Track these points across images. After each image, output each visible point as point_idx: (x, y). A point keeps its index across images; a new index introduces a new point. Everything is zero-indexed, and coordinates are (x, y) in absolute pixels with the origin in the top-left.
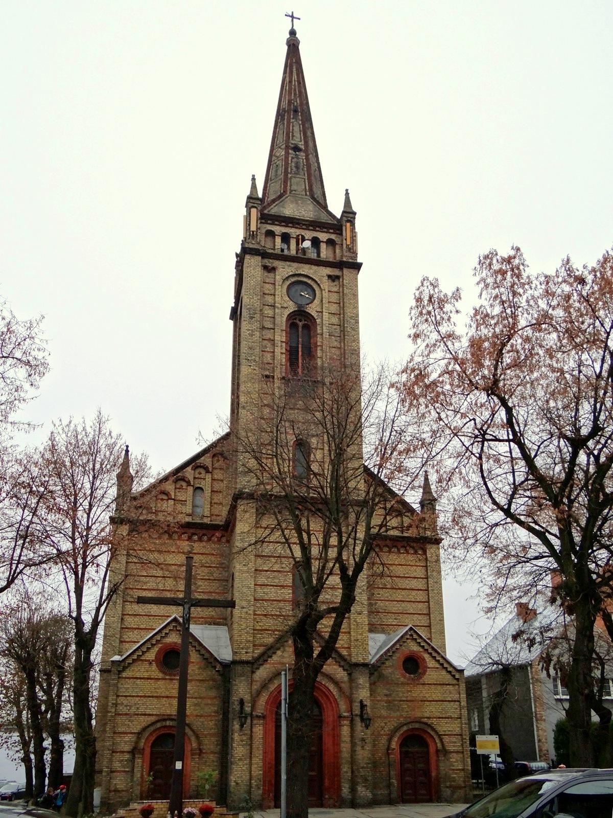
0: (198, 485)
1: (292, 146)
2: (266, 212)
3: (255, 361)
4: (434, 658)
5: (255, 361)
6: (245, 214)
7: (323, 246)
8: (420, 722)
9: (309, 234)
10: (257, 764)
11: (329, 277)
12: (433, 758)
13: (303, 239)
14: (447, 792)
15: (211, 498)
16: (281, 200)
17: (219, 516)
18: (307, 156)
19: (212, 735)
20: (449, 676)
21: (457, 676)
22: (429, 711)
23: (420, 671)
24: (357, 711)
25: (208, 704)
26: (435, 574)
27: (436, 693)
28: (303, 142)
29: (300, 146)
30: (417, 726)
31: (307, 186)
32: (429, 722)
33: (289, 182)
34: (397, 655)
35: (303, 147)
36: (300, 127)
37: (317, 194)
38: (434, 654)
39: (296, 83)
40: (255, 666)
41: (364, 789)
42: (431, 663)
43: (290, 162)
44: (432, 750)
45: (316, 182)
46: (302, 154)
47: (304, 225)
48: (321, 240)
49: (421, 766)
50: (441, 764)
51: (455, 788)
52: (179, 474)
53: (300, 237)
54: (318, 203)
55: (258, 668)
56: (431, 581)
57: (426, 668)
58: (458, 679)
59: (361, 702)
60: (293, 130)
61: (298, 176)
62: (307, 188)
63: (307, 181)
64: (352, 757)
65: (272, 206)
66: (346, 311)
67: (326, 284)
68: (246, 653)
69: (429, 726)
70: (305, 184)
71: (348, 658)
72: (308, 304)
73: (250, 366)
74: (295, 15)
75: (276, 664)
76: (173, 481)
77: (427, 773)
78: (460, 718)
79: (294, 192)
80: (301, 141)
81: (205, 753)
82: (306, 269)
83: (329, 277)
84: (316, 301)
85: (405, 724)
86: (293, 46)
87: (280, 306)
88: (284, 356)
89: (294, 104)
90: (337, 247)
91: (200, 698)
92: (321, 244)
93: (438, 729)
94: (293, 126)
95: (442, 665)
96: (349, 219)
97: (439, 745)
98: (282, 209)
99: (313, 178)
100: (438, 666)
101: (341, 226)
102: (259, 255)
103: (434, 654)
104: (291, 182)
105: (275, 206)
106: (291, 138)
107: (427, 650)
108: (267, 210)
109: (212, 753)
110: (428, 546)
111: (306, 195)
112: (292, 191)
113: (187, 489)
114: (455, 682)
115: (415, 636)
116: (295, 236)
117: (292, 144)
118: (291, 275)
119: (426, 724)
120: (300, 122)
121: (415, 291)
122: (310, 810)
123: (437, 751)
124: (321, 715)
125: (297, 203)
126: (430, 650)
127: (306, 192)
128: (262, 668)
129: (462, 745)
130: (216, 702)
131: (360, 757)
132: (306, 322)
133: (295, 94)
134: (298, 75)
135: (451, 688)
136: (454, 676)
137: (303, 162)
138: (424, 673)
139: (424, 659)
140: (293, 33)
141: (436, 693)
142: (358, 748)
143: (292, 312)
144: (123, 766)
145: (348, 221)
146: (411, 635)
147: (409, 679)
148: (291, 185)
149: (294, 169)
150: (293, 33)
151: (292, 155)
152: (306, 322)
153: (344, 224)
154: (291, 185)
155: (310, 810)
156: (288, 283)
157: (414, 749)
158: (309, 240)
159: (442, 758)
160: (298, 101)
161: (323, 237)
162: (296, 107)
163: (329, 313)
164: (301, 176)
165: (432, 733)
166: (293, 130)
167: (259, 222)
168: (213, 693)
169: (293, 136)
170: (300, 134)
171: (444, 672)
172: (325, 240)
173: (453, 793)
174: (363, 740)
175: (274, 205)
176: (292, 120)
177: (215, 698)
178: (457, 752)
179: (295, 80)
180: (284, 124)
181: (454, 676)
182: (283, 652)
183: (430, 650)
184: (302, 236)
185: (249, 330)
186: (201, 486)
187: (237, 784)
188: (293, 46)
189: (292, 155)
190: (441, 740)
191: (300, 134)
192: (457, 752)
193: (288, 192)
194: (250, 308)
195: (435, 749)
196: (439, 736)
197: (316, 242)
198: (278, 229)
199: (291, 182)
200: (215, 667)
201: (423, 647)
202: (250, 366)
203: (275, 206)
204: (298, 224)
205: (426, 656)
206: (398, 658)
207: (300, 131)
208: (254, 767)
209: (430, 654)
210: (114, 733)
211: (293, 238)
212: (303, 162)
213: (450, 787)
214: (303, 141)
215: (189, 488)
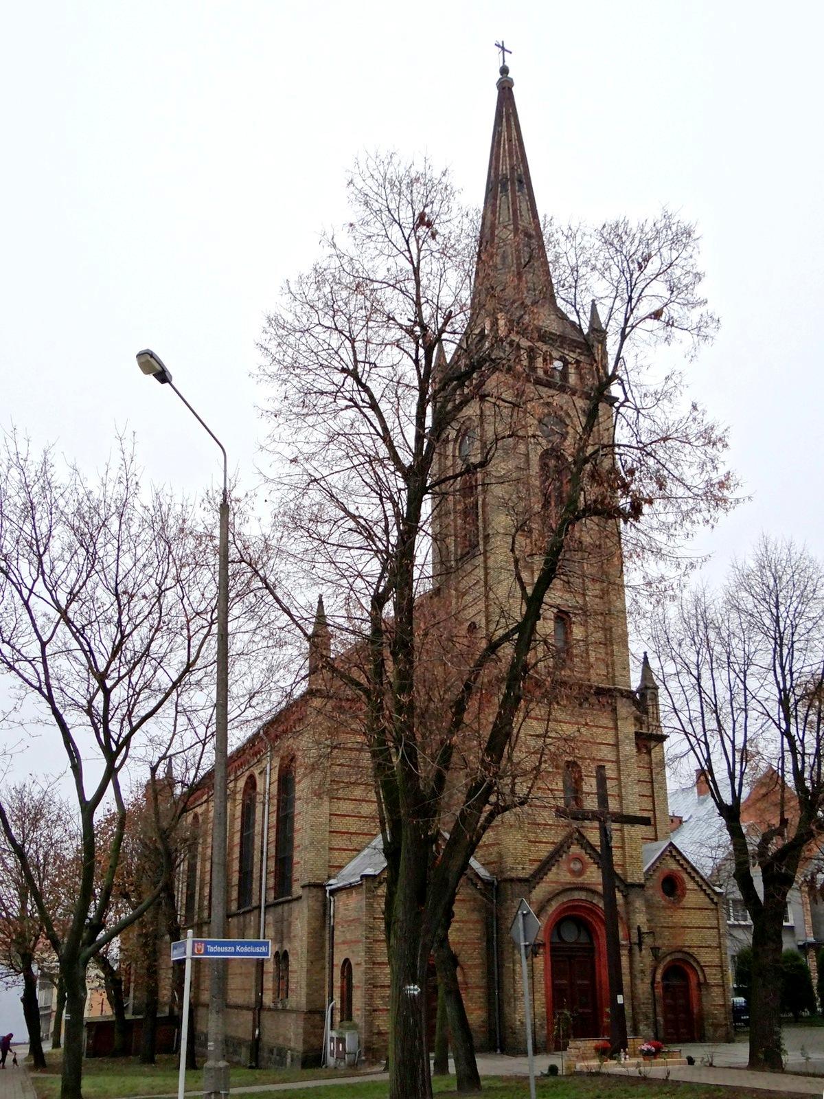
4: (693, 878)
8: (680, 951)
10: (539, 1000)
12: (694, 992)
13: (552, 359)
14: (709, 1031)
19: (476, 966)
20: (707, 900)
21: (715, 900)
22: (691, 939)
23: (679, 892)
24: (635, 939)
25: (470, 929)
26: (660, 777)
27: (696, 919)
30: (679, 956)
32: (691, 951)
34: (657, 874)
38: (693, 874)
40: (532, 885)
41: (645, 1028)
42: (690, 885)
44: (693, 982)
49: (681, 1002)
50: (704, 1000)
51: (716, 1026)
55: (534, 887)
56: (656, 786)
57: (684, 889)
58: (716, 904)
59: (639, 928)
64: (632, 992)
68: (523, 869)
69: (691, 956)
71: (622, 877)
74: (506, 47)
75: (552, 882)
77: (688, 1009)
78: (720, 947)
81: (472, 988)
85: (669, 954)
86: (505, 89)
91: (463, 922)
93: (700, 959)
95: (700, 886)
97: (701, 977)
100: (696, 887)
103: (693, 874)
107: (686, 869)
109: (478, 987)
110: (653, 744)
114: (713, 906)
115: (674, 853)
119: (688, 953)
121: (728, 461)
122: (114, 1018)
123: (699, 985)
124: (592, 943)
126: (689, 870)
128: (537, 888)
129: (722, 977)
130: (479, 926)
131: (640, 991)
133: (517, 157)
135: (708, 913)
136: (712, 899)
138: (684, 895)
139: (682, 880)
140: (504, 71)
141: (696, 919)
142: (638, 982)
144: (385, 1004)
146: (671, 852)
147: (669, 903)
150: (504, 71)
155: (114, 1018)
157: (675, 982)
159: (704, 992)
162: (520, 175)
165: (695, 965)
168: (475, 916)
169: (521, 216)
171: (702, 895)
173: (715, 1031)
174: (642, 972)
176: (518, 194)
177: (477, 922)
178: (718, 986)
180: (507, 196)
181: (712, 899)
182: (558, 869)
183: (689, 870)
187: (522, 1023)
188: (505, 89)
190: (703, 971)
192: (718, 986)
195: (696, 982)
196: (701, 967)
200: (476, 885)
201: (682, 865)
205: (685, 876)
206: (658, 878)
208: (537, 1003)
209: (689, 874)
210: (374, 963)
213: (712, 1025)
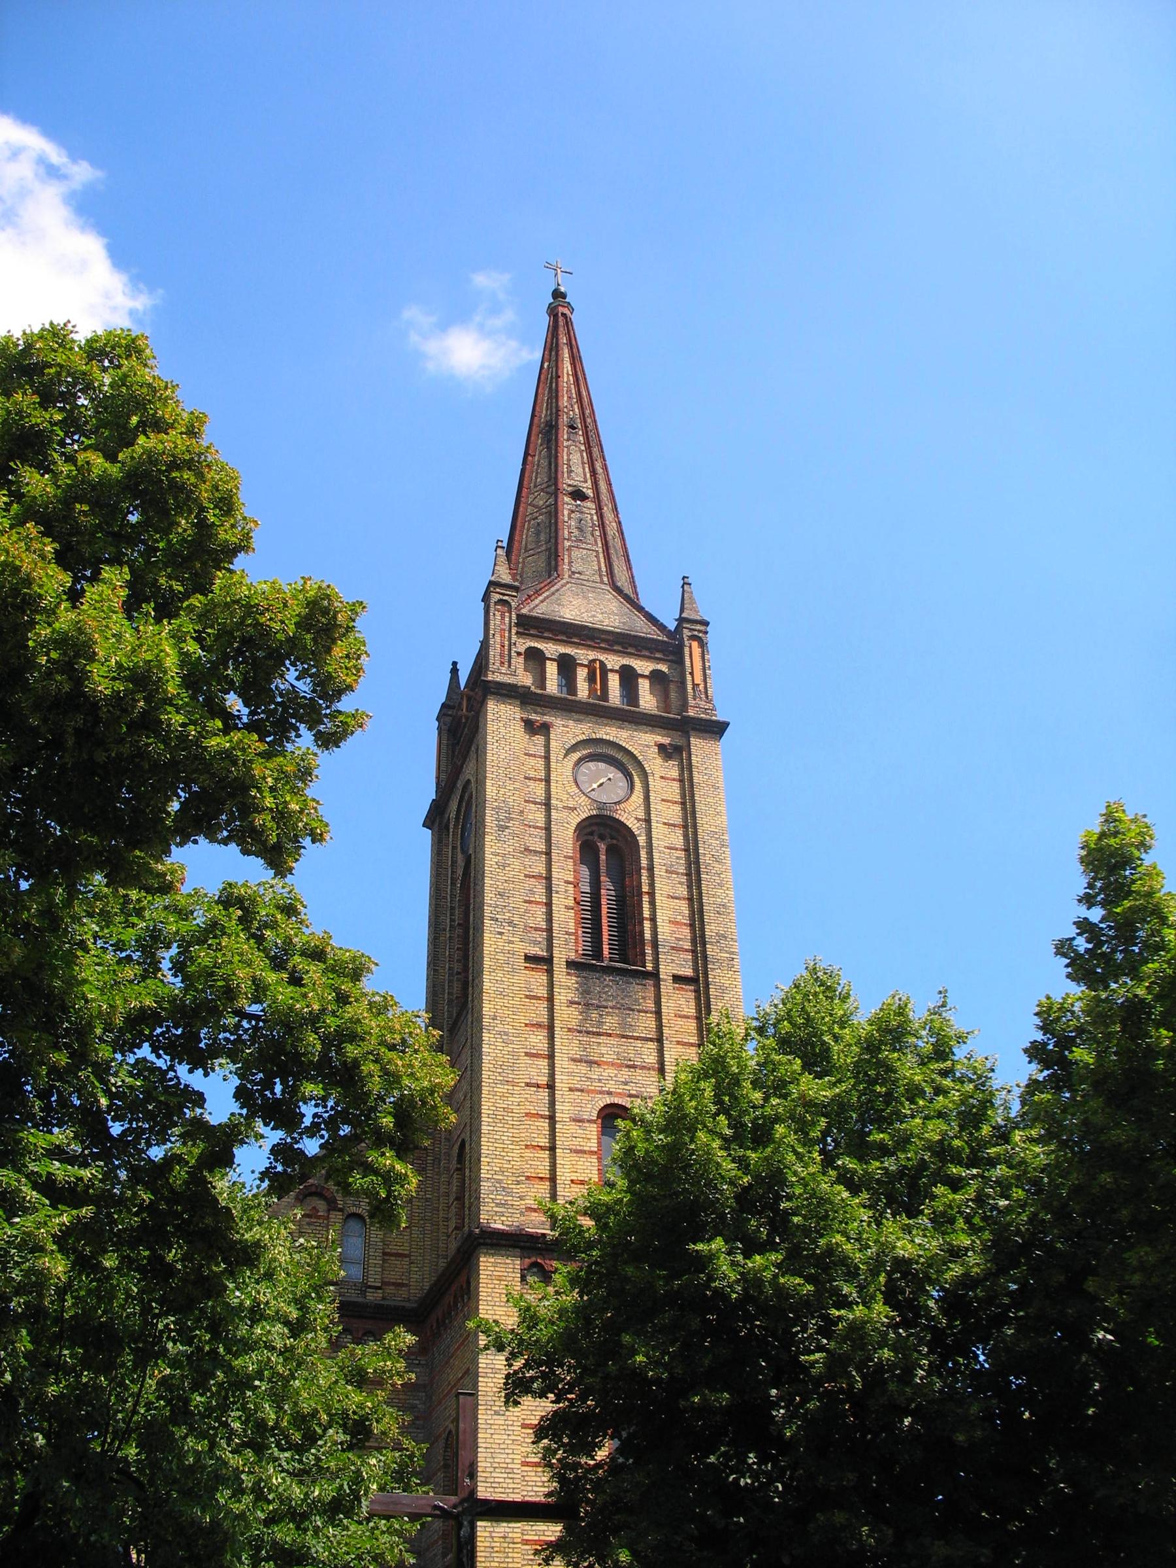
0: (354, 1210)
1: (570, 489)
2: (524, 611)
3: (510, 923)
5: (510, 923)
6: (262, 862)
7: (644, 685)
9: (613, 661)
11: (661, 748)
15: (383, 1241)
16: (553, 589)
17: (402, 1285)
18: (599, 509)
28: (589, 484)
29: (584, 490)
31: (603, 565)
33: (566, 556)
35: (590, 493)
36: (582, 457)
37: (622, 580)
39: (571, 378)
43: (566, 519)
45: (618, 558)
46: (589, 504)
47: (603, 640)
48: (639, 672)
52: (311, 1181)
53: (597, 665)
54: (627, 598)
60: (569, 460)
61: (584, 546)
62: (604, 569)
63: (601, 555)
65: (537, 601)
66: (699, 821)
67: (656, 766)
70: (599, 562)
72: (619, 803)
73: (501, 933)
76: (297, 1198)
79: (577, 575)
80: (586, 482)
82: (610, 732)
83: (661, 748)
84: (634, 798)
87: (560, 805)
88: (571, 913)
89: (567, 413)
90: (672, 686)
92: (640, 680)
94: (569, 454)
96: (696, 633)
98: (557, 608)
99: (612, 551)
101: (681, 646)
102: (515, 697)
104: (570, 556)
105: (542, 602)
106: (566, 475)
108: (527, 608)
111: (602, 582)
112: (574, 573)
113: (328, 1218)
116: (586, 663)
117: (570, 485)
118: (581, 741)
120: (583, 448)
125: (585, 597)
127: (601, 576)
132: (615, 842)
134: (573, 364)
137: (592, 519)
143: (587, 818)
145: (693, 638)
148: (570, 563)
149: (576, 532)
151: (569, 507)
152: (615, 842)
153: (687, 643)
154: (570, 563)
156: (576, 756)
158: (616, 671)
160: (577, 410)
161: (643, 666)
163: (665, 824)
164: (589, 546)
166: (569, 460)
167: (514, 631)
169: (570, 472)
170: (584, 469)
172: (647, 673)
175: (541, 598)
179: (568, 374)
184: (601, 662)
185: (498, 854)
186: (360, 1211)
189: (569, 507)
191: (584, 469)
193: (566, 576)
194: (499, 808)
197: (628, 677)
198: (551, 649)
199: (570, 556)
202: (501, 933)
203: (542, 602)
204: (592, 638)
207: (583, 463)
211: (582, 665)
212: (592, 519)
214: (589, 481)
215: (333, 1214)
